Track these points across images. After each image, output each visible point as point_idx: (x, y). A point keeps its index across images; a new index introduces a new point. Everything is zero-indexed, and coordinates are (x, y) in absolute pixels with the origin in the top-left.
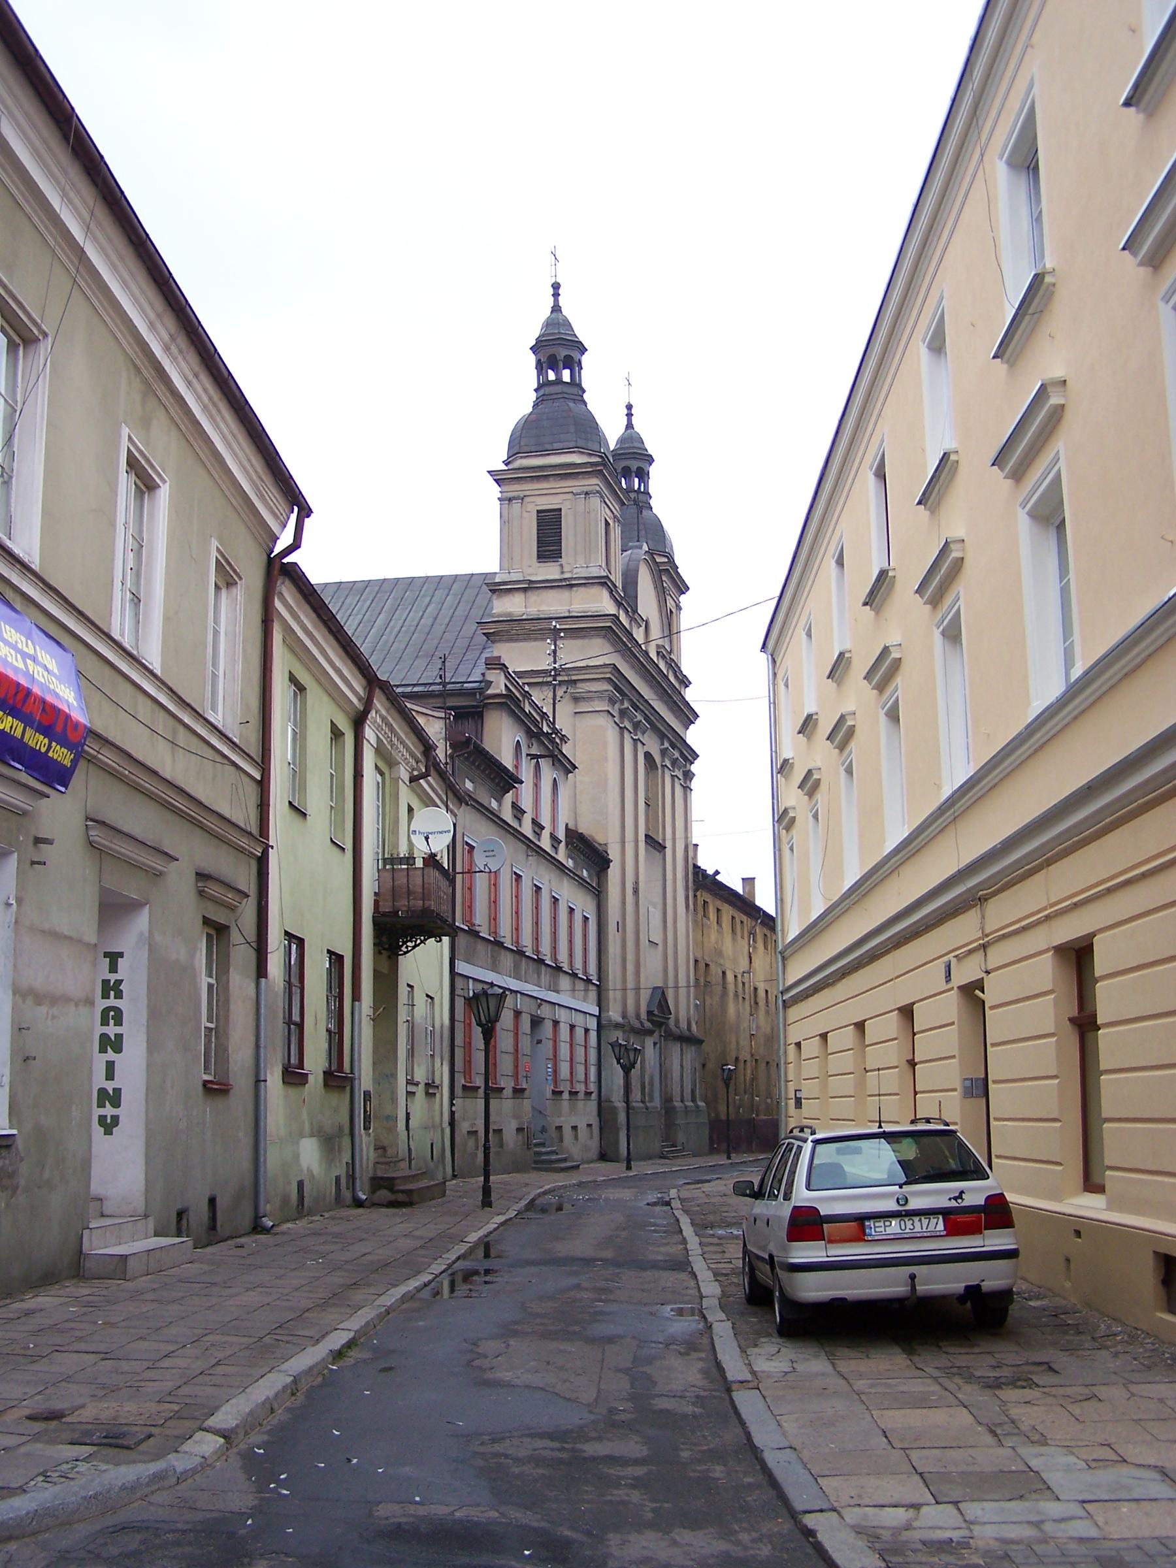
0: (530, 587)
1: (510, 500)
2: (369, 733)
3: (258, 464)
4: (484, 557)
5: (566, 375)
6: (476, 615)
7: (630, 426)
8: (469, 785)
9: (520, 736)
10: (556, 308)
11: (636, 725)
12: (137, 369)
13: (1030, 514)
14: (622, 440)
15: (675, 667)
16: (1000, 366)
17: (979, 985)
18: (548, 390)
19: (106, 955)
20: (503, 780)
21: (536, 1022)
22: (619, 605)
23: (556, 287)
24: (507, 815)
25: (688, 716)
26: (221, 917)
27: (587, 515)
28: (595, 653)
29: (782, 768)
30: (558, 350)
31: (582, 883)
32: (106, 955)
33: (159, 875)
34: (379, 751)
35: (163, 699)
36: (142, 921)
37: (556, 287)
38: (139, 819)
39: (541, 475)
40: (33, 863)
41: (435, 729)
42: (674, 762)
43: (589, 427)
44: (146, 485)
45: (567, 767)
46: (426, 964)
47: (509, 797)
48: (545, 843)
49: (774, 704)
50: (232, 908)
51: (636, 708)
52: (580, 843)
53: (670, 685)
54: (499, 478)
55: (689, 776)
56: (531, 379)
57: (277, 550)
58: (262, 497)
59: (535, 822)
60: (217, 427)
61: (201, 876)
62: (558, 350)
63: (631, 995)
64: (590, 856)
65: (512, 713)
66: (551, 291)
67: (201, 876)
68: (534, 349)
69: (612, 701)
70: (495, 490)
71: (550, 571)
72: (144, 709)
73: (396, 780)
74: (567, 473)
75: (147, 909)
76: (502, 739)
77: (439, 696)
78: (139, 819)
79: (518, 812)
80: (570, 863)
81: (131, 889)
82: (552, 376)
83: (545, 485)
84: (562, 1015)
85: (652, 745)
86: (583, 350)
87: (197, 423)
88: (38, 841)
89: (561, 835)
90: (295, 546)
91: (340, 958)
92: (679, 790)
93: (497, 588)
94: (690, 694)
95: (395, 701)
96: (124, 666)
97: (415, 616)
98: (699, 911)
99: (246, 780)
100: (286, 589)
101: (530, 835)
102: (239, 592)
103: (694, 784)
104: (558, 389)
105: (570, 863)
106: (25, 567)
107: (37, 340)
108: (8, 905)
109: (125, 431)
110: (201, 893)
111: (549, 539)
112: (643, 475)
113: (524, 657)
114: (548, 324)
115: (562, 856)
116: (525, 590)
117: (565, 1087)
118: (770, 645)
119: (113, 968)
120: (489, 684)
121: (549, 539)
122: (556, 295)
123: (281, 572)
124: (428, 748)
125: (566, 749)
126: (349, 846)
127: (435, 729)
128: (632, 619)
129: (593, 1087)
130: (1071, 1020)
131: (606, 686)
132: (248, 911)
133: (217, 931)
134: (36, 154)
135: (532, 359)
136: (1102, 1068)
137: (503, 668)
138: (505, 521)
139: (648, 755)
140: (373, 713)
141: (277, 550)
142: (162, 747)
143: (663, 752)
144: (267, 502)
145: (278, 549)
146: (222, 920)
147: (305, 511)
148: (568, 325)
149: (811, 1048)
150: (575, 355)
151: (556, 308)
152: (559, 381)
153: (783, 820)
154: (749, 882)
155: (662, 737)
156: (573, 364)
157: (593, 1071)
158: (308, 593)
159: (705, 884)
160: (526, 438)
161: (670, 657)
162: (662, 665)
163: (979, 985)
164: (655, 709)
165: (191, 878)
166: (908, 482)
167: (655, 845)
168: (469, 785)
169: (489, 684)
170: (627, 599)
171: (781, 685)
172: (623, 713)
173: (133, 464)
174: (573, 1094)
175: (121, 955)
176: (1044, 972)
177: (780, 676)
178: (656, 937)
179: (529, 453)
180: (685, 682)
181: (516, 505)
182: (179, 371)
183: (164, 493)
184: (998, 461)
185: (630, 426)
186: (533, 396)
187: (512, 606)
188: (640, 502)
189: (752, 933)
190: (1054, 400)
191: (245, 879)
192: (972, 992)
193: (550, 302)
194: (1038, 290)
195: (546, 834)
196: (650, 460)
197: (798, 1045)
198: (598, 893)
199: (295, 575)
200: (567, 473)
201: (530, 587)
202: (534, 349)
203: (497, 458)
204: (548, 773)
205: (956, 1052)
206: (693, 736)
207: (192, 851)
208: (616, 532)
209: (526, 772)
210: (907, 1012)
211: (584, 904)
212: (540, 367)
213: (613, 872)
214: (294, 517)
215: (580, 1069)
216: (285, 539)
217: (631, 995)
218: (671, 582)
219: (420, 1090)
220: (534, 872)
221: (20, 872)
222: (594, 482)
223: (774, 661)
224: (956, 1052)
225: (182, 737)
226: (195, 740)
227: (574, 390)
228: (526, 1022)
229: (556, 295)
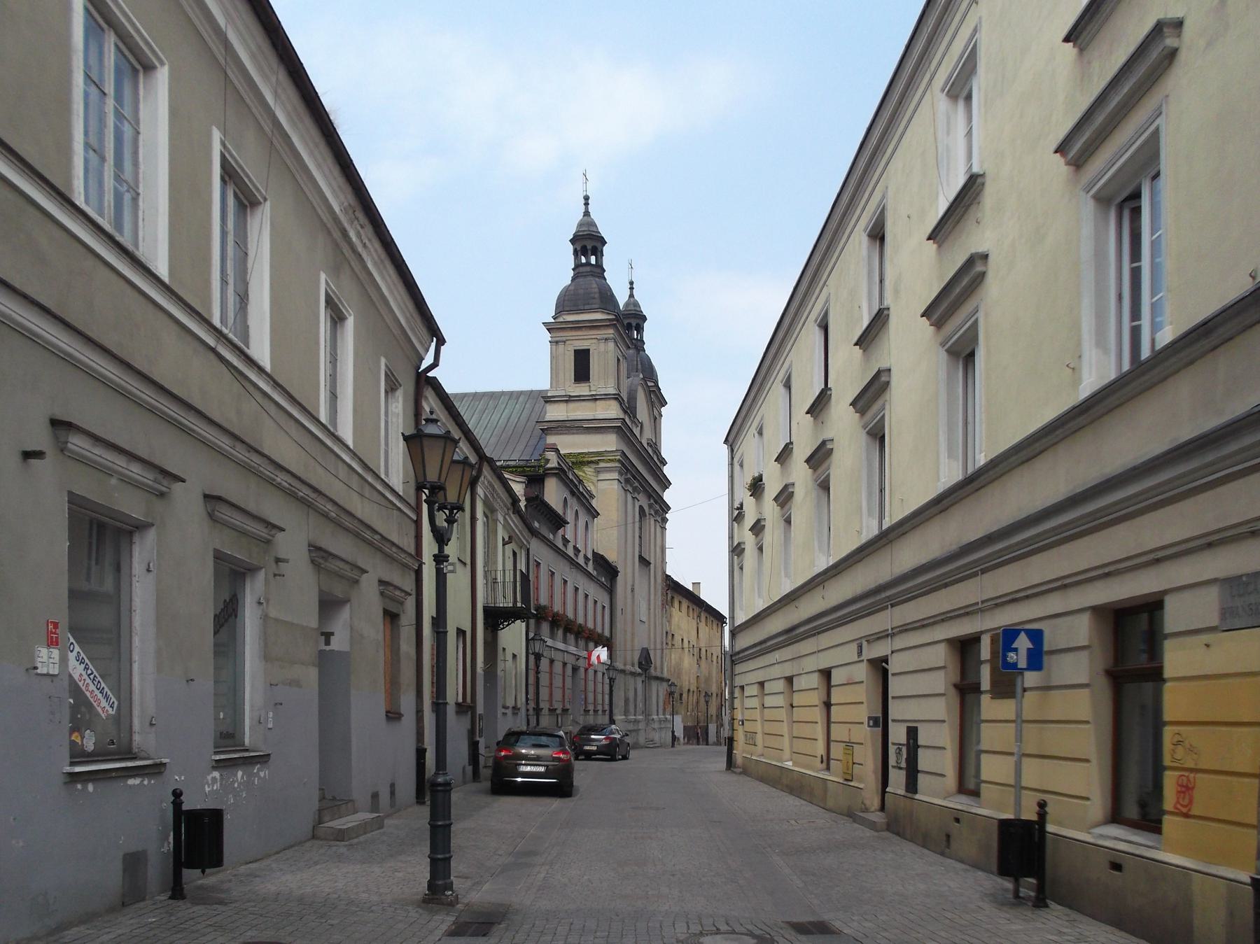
0: (569, 399)
1: (557, 342)
2: (480, 491)
3: (410, 305)
4: (540, 380)
5: (593, 260)
6: (534, 418)
7: (631, 296)
8: (536, 524)
9: (567, 494)
10: (587, 213)
11: (635, 489)
12: (329, 233)
13: (948, 351)
14: (627, 304)
15: (657, 452)
16: (932, 246)
17: (885, 660)
18: (581, 269)
19: (323, 634)
20: (557, 522)
21: (575, 669)
22: (625, 412)
23: (587, 198)
24: (560, 544)
25: (665, 483)
26: (393, 608)
27: (604, 353)
28: (609, 443)
29: (737, 516)
30: (588, 243)
31: (602, 585)
32: (323, 634)
33: (357, 582)
34: (486, 503)
35: (355, 465)
36: (345, 614)
37: (587, 198)
38: (341, 545)
39: (577, 326)
40: (275, 575)
41: (518, 489)
42: (656, 512)
43: (607, 298)
44: (337, 318)
45: (594, 514)
46: (514, 636)
47: (561, 532)
48: (581, 561)
49: (731, 477)
50: (402, 603)
51: (635, 478)
52: (600, 560)
53: (655, 463)
54: (550, 328)
55: (665, 520)
56: (570, 262)
57: (423, 367)
58: (412, 330)
59: (575, 548)
60: (383, 278)
61: (381, 582)
62: (588, 243)
63: (629, 653)
64: (606, 571)
65: (562, 480)
66: (583, 201)
67: (381, 582)
68: (573, 241)
69: (621, 474)
70: (547, 336)
71: (582, 390)
72: (343, 472)
73: (496, 520)
74: (593, 326)
75: (348, 606)
76: (553, 493)
77: (517, 470)
78: (341, 545)
79: (566, 541)
80: (595, 573)
81: (338, 590)
82: (583, 260)
83: (579, 333)
84: (558, 657)
85: (643, 501)
86: (604, 243)
87: (370, 274)
88: (278, 560)
89: (590, 556)
90: (434, 365)
91: (464, 632)
92: (658, 529)
93: (548, 400)
94: (666, 470)
95: (498, 472)
96: (329, 442)
97: (495, 417)
98: (667, 603)
99: (408, 521)
100: (429, 393)
101: (572, 555)
102: (400, 394)
103: (668, 526)
104: (588, 269)
105: (595, 573)
106: (261, 370)
107: (260, 203)
108: (260, 603)
109: (323, 276)
110: (382, 594)
111: (582, 371)
112: (640, 329)
113: (570, 444)
114: (580, 225)
115: (590, 568)
116: (566, 401)
117: (591, 707)
118: (730, 439)
119: (328, 643)
120: (548, 461)
121: (582, 371)
122: (586, 204)
123: (425, 383)
124: (515, 501)
125: (594, 503)
126: (468, 562)
127: (518, 489)
128: (633, 422)
129: (607, 708)
130: (955, 686)
131: (617, 464)
132: (410, 603)
133: (391, 617)
134: (253, 57)
135: (571, 248)
136: (983, 717)
137: (557, 451)
138: (554, 358)
139: (641, 507)
140: (482, 478)
141: (423, 367)
142: (355, 497)
143: (650, 506)
144: (416, 333)
145: (424, 366)
146: (395, 611)
147: (441, 341)
148: (593, 224)
149: (752, 690)
150: (598, 245)
151: (587, 213)
152: (588, 264)
153: (736, 550)
154: (697, 584)
155: (650, 497)
156: (598, 252)
157: (607, 697)
158: (445, 399)
159: (674, 588)
160: (567, 302)
161: (655, 446)
162: (650, 451)
163: (885, 660)
164: (645, 478)
165: (376, 583)
166: (846, 330)
167: (644, 562)
168: (536, 524)
169: (548, 461)
170: (629, 408)
171: (737, 467)
172: (627, 481)
173: (329, 302)
174: (596, 711)
175: (332, 634)
176: (815, 680)
177: (736, 460)
178: (644, 619)
179: (570, 312)
180: (664, 462)
181: (561, 346)
182: (358, 233)
183: (350, 322)
184: (1061, 149)
185: (631, 296)
186: (572, 273)
187: (555, 413)
188: (639, 345)
189: (699, 616)
190: (979, 268)
191: (409, 585)
192: (880, 668)
193: (583, 208)
194: (972, 188)
195: (581, 555)
196: (644, 319)
197: (742, 688)
198: (611, 591)
199: (435, 385)
200: (593, 326)
201: (569, 399)
202: (573, 241)
203: (549, 314)
204: (583, 518)
205: (864, 700)
206: (668, 496)
207: (376, 569)
208: (624, 365)
209: (570, 517)
210: (826, 674)
211: (603, 598)
212: (576, 252)
213: (620, 578)
214: (433, 345)
215: (600, 697)
216: (428, 360)
217: (629, 653)
218: (656, 400)
219: (509, 712)
220: (575, 579)
221: (267, 582)
222: (610, 332)
223: (732, 451)
224: (864, 700)
225: (367, 491)
226: (375, 493)
227: (598, 270)
228: (569, 668)
229: (586, 204)
